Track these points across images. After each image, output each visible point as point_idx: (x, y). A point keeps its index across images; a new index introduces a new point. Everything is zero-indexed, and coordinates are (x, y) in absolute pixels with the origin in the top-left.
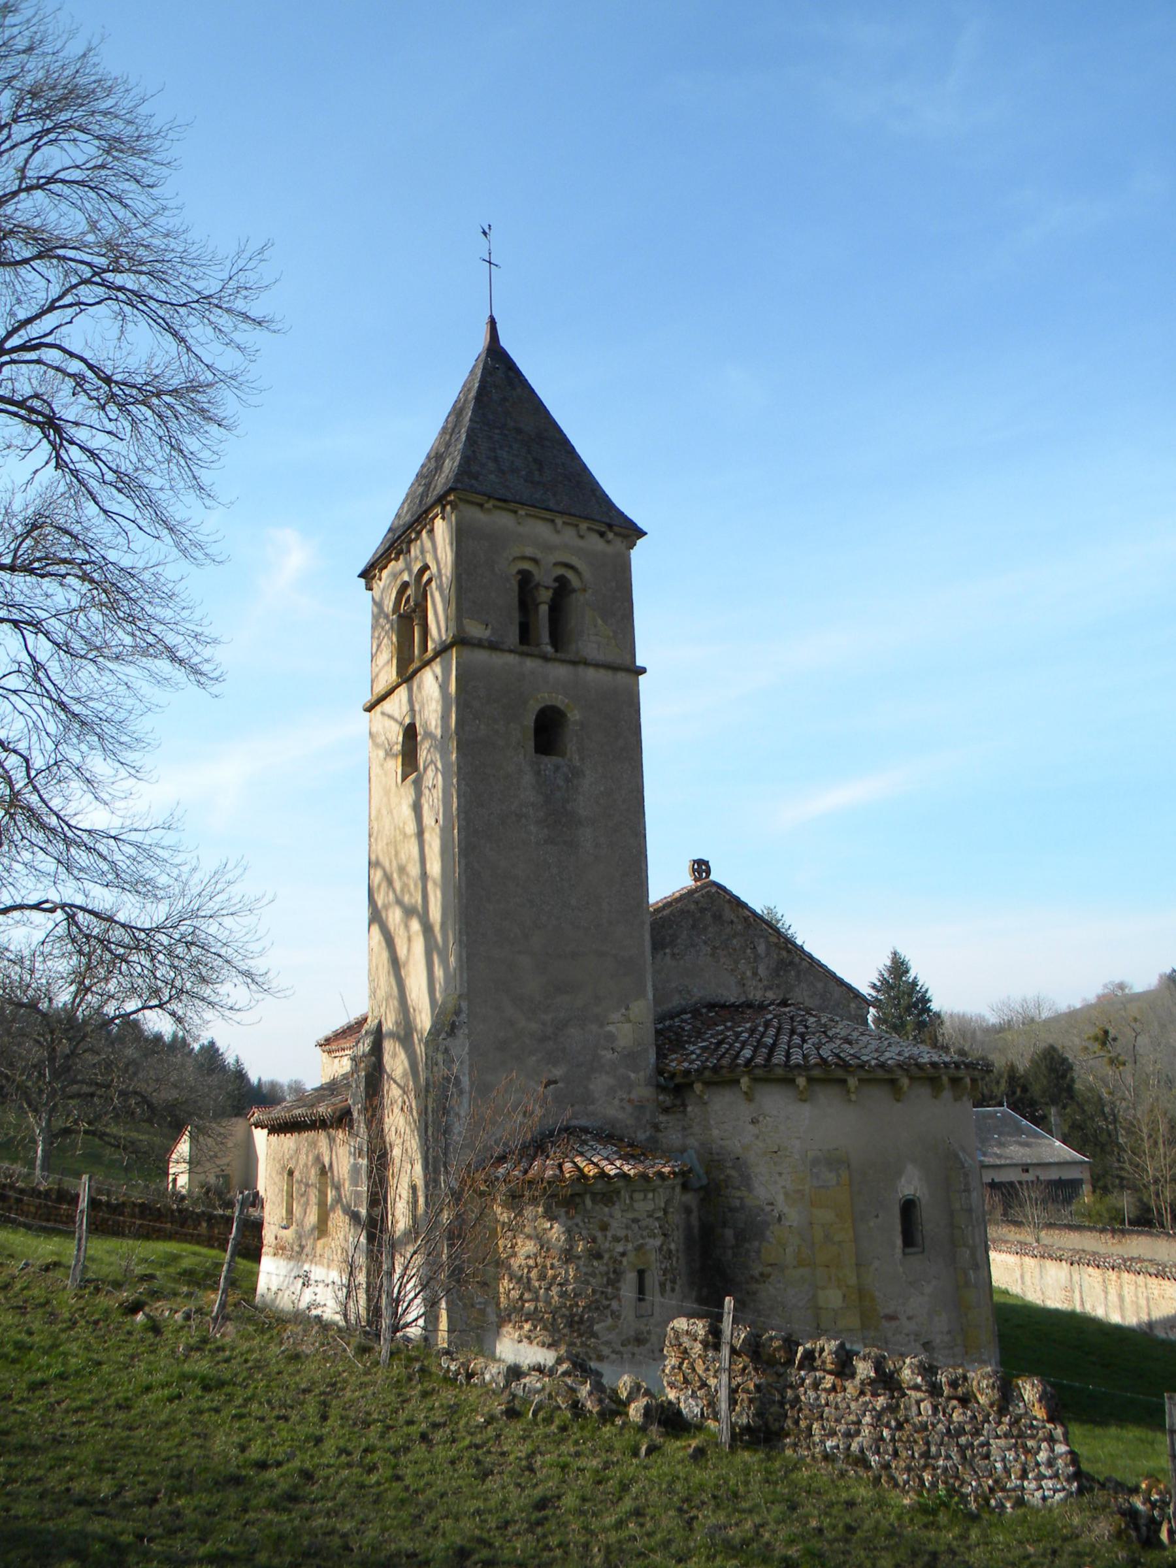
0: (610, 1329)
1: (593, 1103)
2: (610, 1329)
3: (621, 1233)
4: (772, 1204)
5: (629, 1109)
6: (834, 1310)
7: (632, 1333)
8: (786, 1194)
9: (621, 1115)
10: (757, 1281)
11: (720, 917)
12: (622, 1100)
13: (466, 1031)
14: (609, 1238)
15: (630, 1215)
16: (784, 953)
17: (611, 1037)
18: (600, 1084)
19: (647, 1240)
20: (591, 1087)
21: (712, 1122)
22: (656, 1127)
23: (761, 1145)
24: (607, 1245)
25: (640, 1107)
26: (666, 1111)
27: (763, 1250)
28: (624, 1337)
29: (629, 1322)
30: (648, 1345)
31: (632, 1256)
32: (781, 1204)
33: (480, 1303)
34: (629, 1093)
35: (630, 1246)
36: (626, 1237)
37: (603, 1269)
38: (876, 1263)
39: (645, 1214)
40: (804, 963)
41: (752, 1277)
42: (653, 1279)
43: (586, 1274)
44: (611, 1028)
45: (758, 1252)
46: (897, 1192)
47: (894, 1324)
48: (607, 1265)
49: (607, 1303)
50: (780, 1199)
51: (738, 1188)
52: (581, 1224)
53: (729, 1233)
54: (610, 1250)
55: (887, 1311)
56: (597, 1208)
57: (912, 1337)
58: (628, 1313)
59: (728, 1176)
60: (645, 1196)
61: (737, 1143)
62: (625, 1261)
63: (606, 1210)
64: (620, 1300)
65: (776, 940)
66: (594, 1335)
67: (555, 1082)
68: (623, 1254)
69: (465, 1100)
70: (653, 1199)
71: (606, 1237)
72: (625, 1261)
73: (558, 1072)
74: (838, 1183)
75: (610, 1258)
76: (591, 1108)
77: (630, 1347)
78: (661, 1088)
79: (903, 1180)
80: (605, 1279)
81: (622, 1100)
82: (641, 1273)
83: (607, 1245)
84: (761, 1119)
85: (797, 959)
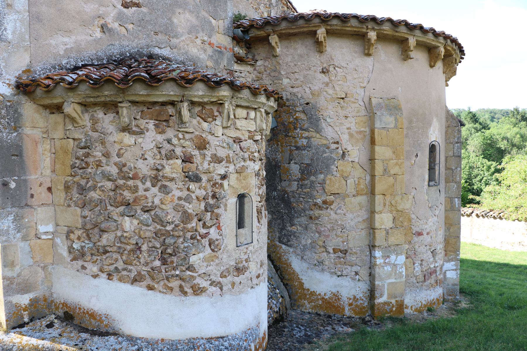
0: (205, 259)
1: (176, 36)
2: (208, 260)
3: (222, 153)
4: (337, 143)
5: (210, 51)
6: (385, 229)
7: (233, 263)
8: (351, 135)
9: (203, 56)
10: (320, 208)
20: (175, 21)
21: (283, 73)
23: (331, 91)
24: (206, 165)
25: (219, 51)
26: (240, 60)
27: (328, 182)
30: (247, 274)
32: (346, 144)
33: (46, 233)
34: (210, 37)
35: (232, 168)
37: (201, 193)
39: (247, 135)
41: (316, 204)
43: (180, 199)
45: (324, 182)
48: (205, 189)
49: (203, 231)
51: (306, 130)
52: (175, 141)
53: (295, 168)
54: (208, 172)
56: (195, 122)
58: (229, 242)
59: (296, 119)
61: (307, 90)
62: (225, 183)
66: (191, 268)
68: (224, 177)
70: (255, 119)
71: (204, 156)
75: (209, 181)
76: (174, 41)
77: (229, 278)
78: (236, 39)
80: (203, 205)
81: (203, 42)
82: (241, 197)
84: (331, 69)
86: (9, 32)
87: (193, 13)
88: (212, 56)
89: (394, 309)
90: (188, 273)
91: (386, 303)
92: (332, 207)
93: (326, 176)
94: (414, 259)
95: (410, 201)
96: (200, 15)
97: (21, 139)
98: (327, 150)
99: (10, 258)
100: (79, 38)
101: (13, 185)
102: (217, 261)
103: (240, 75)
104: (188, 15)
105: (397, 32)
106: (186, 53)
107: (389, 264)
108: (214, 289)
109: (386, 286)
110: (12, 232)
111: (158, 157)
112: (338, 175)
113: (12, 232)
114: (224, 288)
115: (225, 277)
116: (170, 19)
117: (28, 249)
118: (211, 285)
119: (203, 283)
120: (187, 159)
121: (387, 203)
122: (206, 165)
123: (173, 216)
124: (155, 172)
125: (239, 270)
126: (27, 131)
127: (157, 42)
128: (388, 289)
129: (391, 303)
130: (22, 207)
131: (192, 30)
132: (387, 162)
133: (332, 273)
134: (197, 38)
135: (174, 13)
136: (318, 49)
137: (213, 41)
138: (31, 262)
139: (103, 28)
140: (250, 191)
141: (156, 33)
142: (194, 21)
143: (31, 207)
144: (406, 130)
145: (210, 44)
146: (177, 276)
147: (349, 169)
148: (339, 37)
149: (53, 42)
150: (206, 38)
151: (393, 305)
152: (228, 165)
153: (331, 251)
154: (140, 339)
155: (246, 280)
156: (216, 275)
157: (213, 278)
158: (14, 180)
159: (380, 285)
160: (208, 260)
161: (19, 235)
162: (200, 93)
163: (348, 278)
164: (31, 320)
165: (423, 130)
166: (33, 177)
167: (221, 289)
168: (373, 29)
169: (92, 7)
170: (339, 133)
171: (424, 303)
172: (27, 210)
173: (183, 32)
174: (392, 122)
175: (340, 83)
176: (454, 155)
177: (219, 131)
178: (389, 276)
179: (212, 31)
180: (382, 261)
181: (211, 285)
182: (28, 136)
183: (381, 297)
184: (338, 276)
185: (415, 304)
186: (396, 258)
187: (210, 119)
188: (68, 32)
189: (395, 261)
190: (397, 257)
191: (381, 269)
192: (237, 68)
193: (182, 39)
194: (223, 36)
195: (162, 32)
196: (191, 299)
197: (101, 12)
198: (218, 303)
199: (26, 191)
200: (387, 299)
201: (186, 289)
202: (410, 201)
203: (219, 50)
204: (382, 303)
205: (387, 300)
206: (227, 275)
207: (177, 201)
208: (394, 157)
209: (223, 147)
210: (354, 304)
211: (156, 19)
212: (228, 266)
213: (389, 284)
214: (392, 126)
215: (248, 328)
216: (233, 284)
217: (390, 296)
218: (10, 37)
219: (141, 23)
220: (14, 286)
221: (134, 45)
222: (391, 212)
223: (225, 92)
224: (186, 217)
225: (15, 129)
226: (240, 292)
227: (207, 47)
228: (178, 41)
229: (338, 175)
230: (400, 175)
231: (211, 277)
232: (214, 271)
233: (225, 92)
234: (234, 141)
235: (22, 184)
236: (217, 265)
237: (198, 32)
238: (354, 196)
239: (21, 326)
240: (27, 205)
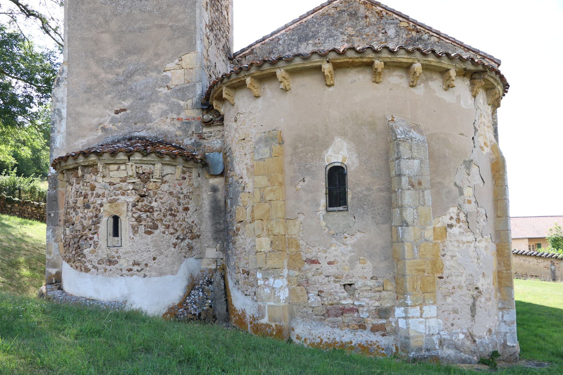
1: (150, 121)
2: (92, 252)
3: (100, 192)
5: (178, 124)
8: (247, 169)
9: (172, 129)
11: (356, 14)
12: (173, 119)
13: (66, 83)
14: (94, 195)
15: (107, 180)
16: (414, 33)
17: (168, 79)
18: (155, 110)
19: (120, 196)
20: (150, 111)
22: (201, 137)
27: (237, 211)
28: (99, 259)
29: (103, 252)
30: (117, 266)
31: (106, 207)
34: (179, 114)
36: (104, 194)
37: (90, 214)
38: (301, 218)
40: (433, 39)
42: (125, 224)
43: (82, 218)
44: (168, 74)
46: (323, 159)
47: (315, 266)
48: (91, 211)
50: (245, 172)
55: (309, 256)
57: (332, 279)
60: (119, 168)
63: (94, 177)
64: (98, 235)
65: (406, 25)
66: (84, 256)
67: (124, 110)
68: (101, 205)
69: (64, 123)
71: (92, 194)
72: (102, 209)
73: (126, 104)
74: (271, 156)
75: (93, 208)
76: (149, 125)
79: (330, 150)
80: (91, 221)
82: (116, 219)
83: (92, 199)
85: (426, 36)
86: (58, 144)
87: (163, 102)
88: (181, 127)
89: (274, 333)
90: (83, 259)
91: (268, 325)
92: (239, 233)
93: (236, 207)
94: (308, 288)
95: (297, 227)
96: (170, 102)
97: (57, 193)
98: (238, 185)
99: (50, 250)
100: (90, 138)
101: (52, 215)
102: (95, 254)
103: (210, 135)
104: (160, 105)
105: (263, 71)
106: (159, 130)
107: (268, 286)
108: (94, 270)
109: (266, 307)
110: (51, 237)
111: (75, 196)
112: (242, 205)
113: (51, 237)
114: (99, 271)
115: (100, 264)
116: (146, 112)
117: (57, 246)
118: (93, 267)
119: (90, 266)
120: (85, 196)
121: (265, 228)
122: (92, 199)
123: (79, 227)
124: (74, 204)
125: (111, 262)
126: (60, 189)
127: (136, 128)
128: (268, 312)
129: (272, 326)
130: (55, 226)
131: (164, 114)
132: (263, 189)
133: (243, 292)
134: (167, 118)
135: (149, 107)
136: (374, 79)
137: (181, 116)
138: (58, 253)
139: (104, 129)
140: (121, 214)
141: (135, 124)
142: (165, 107)
143: (59, 226)
144: (290, 157)
145: (178, 119)
146: (80, 260)
147: (247, 199)
148: (242, 88)
149: (76, 144)
150: (175, 116)
151: (273, 328)
152: (102, 198)
153: (242, 272)
154: (65, 292)
155: (115, 269)
156: (95, 262)
157: (94, 264)
158: (53, 213)
159: (262, 305)
160: (92, 252)
161: (53, 239)
162: (82, 161)
163: (250, 298)
164: (56, 283)
165: (315, 153)
166: (61, 211)
167: (98, 270)
168: (247, 76)
169: (96, 120)
170: (242, 169)
171: (325, 340)
172: (57, 227)
173: (156, 117)
174: (267, 152)
175: (241, 127)
176: (396, 175)
177: (100, 180)
178: (269, 298)
179: (180, 109)
180: (262, 282)
181: (93, 267)
182: (60, 191)
183: (263, 318)
184: (246, 295)
185: (311, 338)
186: (274, 282)
187: (96, 174)
188: (84, 136)
189: (273, 284)
190: (274, 280)
191: (262, 290)
192: (207, 131)
193: (155, 122)
194: (192, 110)
195: (139, 122)
196: (83, 274)
197: (101, 121)
198: (95, 279)
199: (58, 218)
200: (269, 321)
201: (82, 268)
202: (297, 227)
203: (187, 121)
204: (264, 324)
205: (268, 322)
206: (102, 263)
207: (80, 219)
208: (269, 184)
209: (102, 188)
210: (253, 323)
211: (136, 115)
212: (102, 258)
213: (269, 306)
214: (267, 156)
215: (115, 300)
216: (106, 270)
217: (271, 319)
218: (58, 146)
219: (126, 120)
220: (50, 264)
221: (121, 134)
222: (268, 235)
223: (93, 158)
224: (84, 228)
225: (55, 189)
226: (110, 276)
227: (176, 122)
228: (152, 124)
229: (242, 205)
230: (274, 201)
231: (93, 263)
232: (94, 259)
233: (93, 158)
234: (110, 184)
235: (56, 214)
236: (96, 256)
237: (168, 114)
238: (250, 223)
239: (51, 284)
240: (57, 225)
